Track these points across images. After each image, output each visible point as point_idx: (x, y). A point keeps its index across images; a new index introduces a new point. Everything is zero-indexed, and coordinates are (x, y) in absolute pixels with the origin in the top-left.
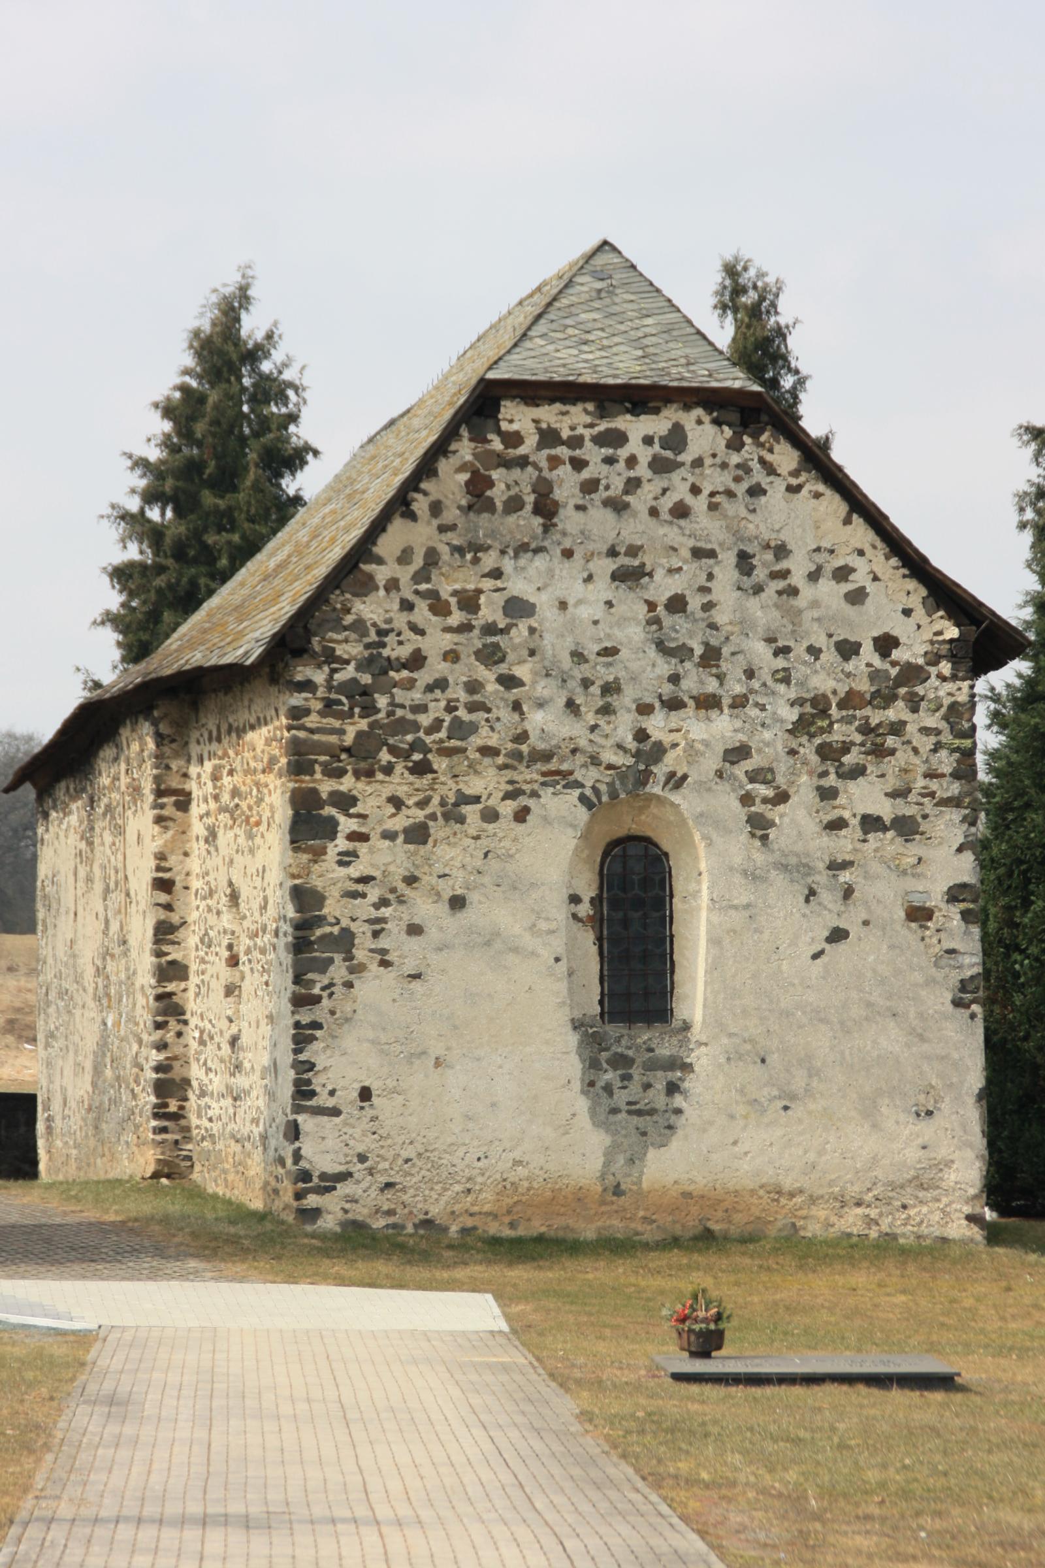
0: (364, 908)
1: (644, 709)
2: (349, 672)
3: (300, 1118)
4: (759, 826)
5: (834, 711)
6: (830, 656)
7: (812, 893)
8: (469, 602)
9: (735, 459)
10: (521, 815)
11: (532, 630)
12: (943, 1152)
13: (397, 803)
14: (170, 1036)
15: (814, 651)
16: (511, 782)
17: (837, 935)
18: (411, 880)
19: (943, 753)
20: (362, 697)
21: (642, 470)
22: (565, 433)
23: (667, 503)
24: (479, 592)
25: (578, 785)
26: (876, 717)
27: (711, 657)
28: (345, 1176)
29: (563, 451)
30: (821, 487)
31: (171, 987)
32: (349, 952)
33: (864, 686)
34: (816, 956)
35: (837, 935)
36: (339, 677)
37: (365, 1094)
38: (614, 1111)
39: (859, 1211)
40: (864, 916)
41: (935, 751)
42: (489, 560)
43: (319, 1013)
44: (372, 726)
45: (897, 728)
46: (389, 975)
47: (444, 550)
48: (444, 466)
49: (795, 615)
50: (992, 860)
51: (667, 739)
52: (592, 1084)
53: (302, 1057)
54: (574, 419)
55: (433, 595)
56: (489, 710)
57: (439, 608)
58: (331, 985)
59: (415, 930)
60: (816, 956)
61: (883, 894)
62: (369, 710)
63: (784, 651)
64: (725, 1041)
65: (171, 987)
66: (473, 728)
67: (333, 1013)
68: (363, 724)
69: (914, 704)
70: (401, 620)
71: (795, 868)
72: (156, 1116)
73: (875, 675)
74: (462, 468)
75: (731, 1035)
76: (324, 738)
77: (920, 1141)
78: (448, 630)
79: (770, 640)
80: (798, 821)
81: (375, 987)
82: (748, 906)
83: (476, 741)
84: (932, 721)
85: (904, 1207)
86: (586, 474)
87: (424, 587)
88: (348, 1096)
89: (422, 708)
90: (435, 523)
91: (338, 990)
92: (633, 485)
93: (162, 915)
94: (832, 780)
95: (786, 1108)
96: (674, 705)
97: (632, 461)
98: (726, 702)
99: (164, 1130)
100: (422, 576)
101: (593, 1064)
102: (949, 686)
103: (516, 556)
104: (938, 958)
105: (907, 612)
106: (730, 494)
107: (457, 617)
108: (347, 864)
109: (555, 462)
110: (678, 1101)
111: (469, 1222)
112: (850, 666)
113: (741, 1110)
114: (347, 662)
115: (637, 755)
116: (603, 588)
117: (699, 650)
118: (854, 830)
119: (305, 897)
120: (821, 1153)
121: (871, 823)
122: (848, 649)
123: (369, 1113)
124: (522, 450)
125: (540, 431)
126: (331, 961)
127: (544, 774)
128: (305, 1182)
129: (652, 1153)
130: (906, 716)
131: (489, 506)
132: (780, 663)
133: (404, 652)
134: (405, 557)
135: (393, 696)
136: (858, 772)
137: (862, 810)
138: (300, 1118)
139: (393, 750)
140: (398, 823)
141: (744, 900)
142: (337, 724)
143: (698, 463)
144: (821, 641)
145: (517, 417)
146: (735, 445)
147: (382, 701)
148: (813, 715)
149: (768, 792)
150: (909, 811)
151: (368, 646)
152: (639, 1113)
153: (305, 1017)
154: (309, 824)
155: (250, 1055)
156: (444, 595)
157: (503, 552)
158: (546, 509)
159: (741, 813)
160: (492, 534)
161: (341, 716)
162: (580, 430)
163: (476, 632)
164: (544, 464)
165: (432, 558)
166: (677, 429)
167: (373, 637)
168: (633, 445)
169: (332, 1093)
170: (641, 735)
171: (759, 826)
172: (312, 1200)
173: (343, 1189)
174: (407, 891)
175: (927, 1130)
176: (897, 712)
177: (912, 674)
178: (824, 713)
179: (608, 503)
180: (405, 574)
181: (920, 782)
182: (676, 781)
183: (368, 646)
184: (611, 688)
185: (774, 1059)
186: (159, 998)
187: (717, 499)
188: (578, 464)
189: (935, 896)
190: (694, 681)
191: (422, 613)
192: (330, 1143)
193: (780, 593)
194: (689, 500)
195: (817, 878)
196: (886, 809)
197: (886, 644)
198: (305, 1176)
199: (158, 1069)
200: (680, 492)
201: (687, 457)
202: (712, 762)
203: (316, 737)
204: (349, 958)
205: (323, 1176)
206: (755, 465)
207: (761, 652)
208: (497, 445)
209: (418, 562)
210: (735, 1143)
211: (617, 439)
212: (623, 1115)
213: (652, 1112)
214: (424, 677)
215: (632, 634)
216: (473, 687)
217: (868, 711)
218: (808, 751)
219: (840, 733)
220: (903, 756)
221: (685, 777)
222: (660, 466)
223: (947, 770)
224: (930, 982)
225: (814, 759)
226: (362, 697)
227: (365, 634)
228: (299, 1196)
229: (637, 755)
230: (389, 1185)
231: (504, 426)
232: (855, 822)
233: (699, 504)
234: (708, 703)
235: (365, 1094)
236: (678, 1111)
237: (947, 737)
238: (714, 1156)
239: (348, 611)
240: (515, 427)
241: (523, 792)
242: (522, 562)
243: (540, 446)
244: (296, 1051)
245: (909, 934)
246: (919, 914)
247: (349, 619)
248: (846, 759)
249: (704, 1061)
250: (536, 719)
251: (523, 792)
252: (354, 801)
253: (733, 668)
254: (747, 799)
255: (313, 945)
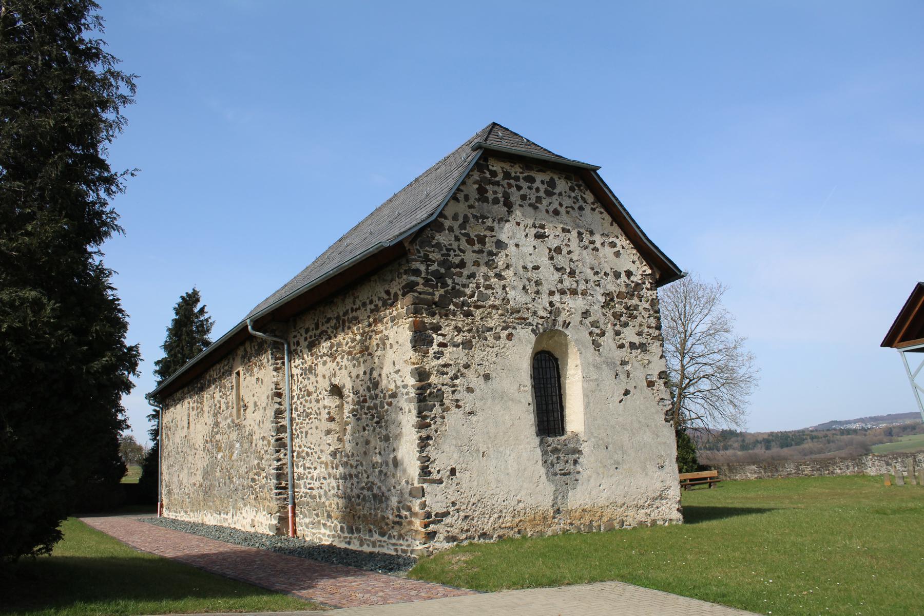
0: (446, 379)
1: (552, 293)
2: (434, 267)
3: (425, 486)
4: (597, 345)
5: (615, 299)
6: (611, 278)
8: (482, 240)
9: (573, 195)
10: (510, 337)
11: (507, 255)
12: (667, 483)
13: (458, 330)
14: (282, 456)
15: (606, 274)
16: (504, 322)
17: (627, 393)
18: (467, 366)
19: (652, 318)
20: (440, 278)
21: (542, 194)
22: (513, 175)
23: (551, 209)
24: (485, 236)
25: (530, 325)
26: (630, 303)
27: (572, 273)
28: (446, 514)
29: (512, 181)
30: (602, 210)
31: (282, 435)
32: (442, 401)
33: (623, 289)
34: (620, 402)
35: (627, 393)
36: (431, 268)
37: (453, 472)
38: (556, 474)
39: (643, 511)
42: (489, 223)
43: (431, 431)
44: (446, 292)
45: (636, 308)
46: (460, 412)
48: (470, 181)
49: (596, 257)
51: (561, 306)
52: (545, 462)
53: (424, 454)
54: (515, 170)
55: (467, 235)
56: (493, 289)
57: (470, 242)
58: (435, 417)
59: (470, 390)
60: (620, 402)
62: (444, 285)
63: (597, 273)
65: (282, 435)
66: (488, 298)
67: (436, 431)
68: (442, 291)
69: (640, 298)
70: (455, 245)
71: (610, 363)
72: (277, 488)
73: (627, 285)
74: (475, 183)
76: (426, 296)
78: (474, 252)
79: (592, 269)
80: (608, 341)
81: (454, 417)
82: (596, 380)
83: (489, 303)
84: (647, 306)
86: (522, 192)
87: (463, 231)
88: (445, 473)
89: (464, 286)
90: (467, 204)
91: (439, 420)
92: (539, 200)
93: (277, 406)
94: (617, 327)
96: (562, 292)
97: (538, 190)
98: (580, 292)
99: (280, 494)
100: (463, 226)
101: (545, 453)
102: (650, 292)
103: (499, 223)
105: (634, 262)
106: (573, 208)
107: (477, 247)
108: (438, 358)
109: (510, 186)
110: (579, 468)
111: (501, 532)
112: (618, 281)
113: (601, 470)
114: (434, 262)
115: (550, 313)
116: (532, 241)
117: (568, 270)
118: (627, 349)
119: (422, 375)
120: (629, 487)
121: (633, 346)
122: (617, 275)
123: (455, 481)
124: (497, 179)
125: (503, 172)
126: (434, 405)
127: (515, 319)
128: (428, 518)
130: (639, 303)
131: (486, 200)
132: (596, 278)
133: (457, 260)
134: (455, 217)
135: (454, 280)
136: (626, 325)
138: (425, 486)
139: (455, 305)
140: (459, 339)
141: (594, 377)
142: (431, 291)
143: (560, 194)
144: (608, 271)
145: (496, 166)
146: (572, 189)
147: (449, 281)
148: (609, 298)
149: (598, 331)
150: (644, 341)
151: (443, 255)
152: (564, 474)
153: (424, 433)
154: (421, 339)
156: (472, 236)
157: (494, 221)
158: (509, 205)
159: (590, 339)
160: (489, 212)
161: (432, 287)
162: (518, 174)
163: (485, 254)
164: (506, 186)
165: (466, 219)
166: (552, 179)
167: (444, 251)
168: (538, 184)
169: (438, 472)
170: (551, 304)
171: (597, 345)
172: (432, 528)
173: (448, 520)
174: (465, 371)
176: (635, 301)
177: (638, 286)
178: (612, 300)
179: (530, 205)
180: (456, 225)
181: (646, 330)
183: (443, 255)
185: (610, 447)
186: (277, 440)
187: (569, 209)
188: (519, 188)
190: (568, 283)
191: (463, 243)
192: (439, 498)
194: (559, 208)
196: (636, 340)
197: (629, 274)
198: (428, 515)
199: (277, 469)
200: (555, 205)
201: (557, 191)
202: (577, 318)
203: (422, 296)
204: (442, 405)
205: (436, 515)
207: (590, 273)
208: (488, 175)
209: (461, 220)
211: (531, 180)
212: (559, 476)
213: (569, 474)
214: (466, 272)
215: (544, 261)
216: (487, 278)
217: (626, 300)
218: (609, 315)
219: (619, 308)
220: (639, 319)
221: (569, 323)
222: (549, 194)
224: (657, 412)
226: (440, 278)
227: (442, 250)
228: (426, 526)
229: (550, 313)
230: (466, 517)
231: (490, 167)
232: (627, 345)
233: (562, 210)
234: (574, 292)
235: (453, 472)
236: (579, 472)
237: (652, 312)
239: (434, 238)
240: (494, 168)
241: (509, 327)
242: (501, 225)
243: (504, 179)
244: (421, 452)
245: (648, 391)
247: (434, 242)
248: (622, 319)
249: (586, 449)
250: (512, 294)
251: (509, 327)
252: (440, 328)
254: (591, 333)
255: (427, 397)
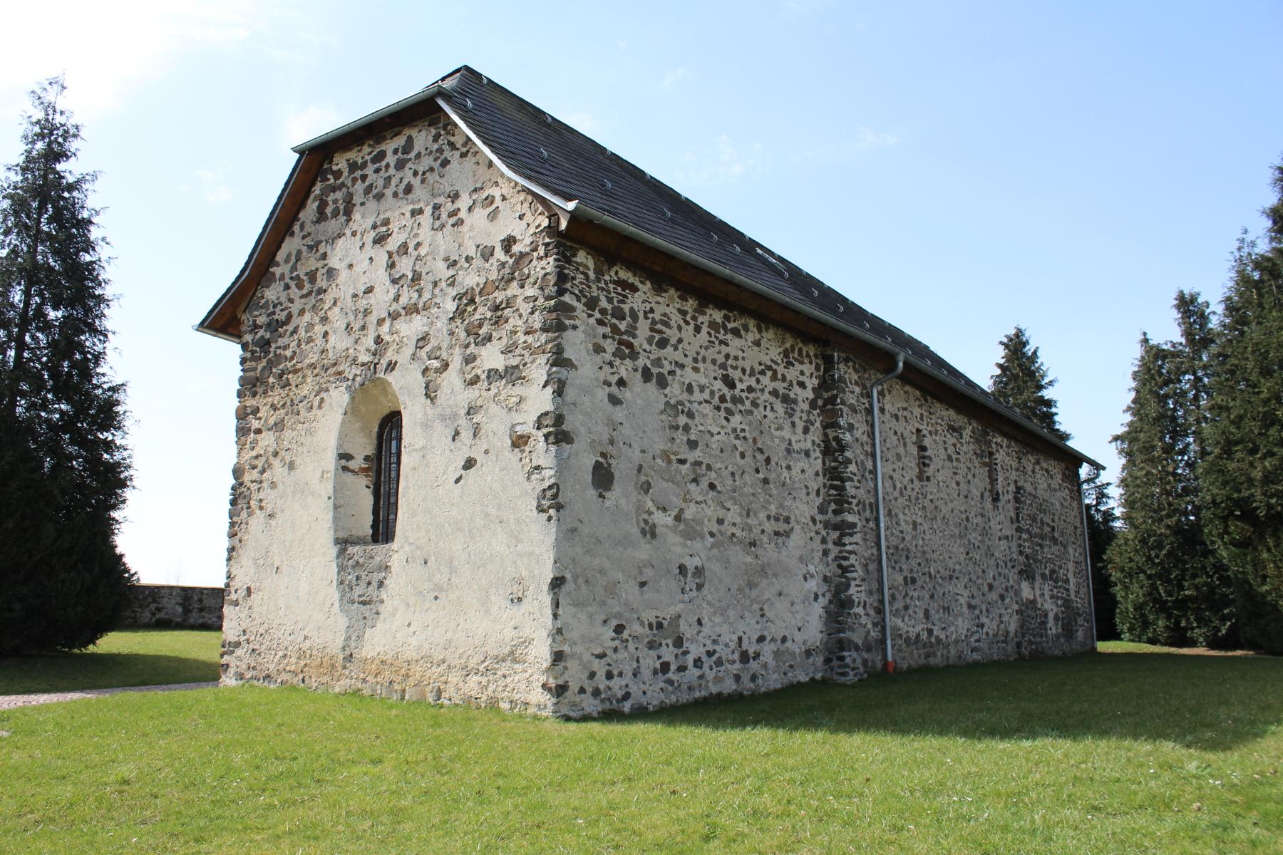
6: (478, 262)
7: (457, 433)
12: (526, 632)
15: (468, 259)
17: (469, 464)
34: (457, 481)
35: (469, 464)
40: (485, 447)
41: (532, 313)
45: (509, 303)
47: (304, 249)
50: (516, 333)
60: (457, 481)
61: (497, 424)
64: (407, 548)
75: (410, 544)
77: (513, 623)
80: (451, 381)
85: (505, 677)
95: (436, 598)
101: (341, 568)
104: (530, 474)
122: (487, 254)
129: (368, 632)
136: (489, 338)
137: (487, 367)
144: (472, 251)
155: (454, 678)
159: (421, 381)
175: (518, 613)
176: (514, 289)
182: (391, 366)
183: (269, 315)
184: (367, 312)
185: (432, 560)
189: (528, 428)
193: (453, 226)
195: (460, 422)
206: (446, 147)
210: (409, 625)
215: (380, 277)
223: (538, 325)
225: (463, 335)
238: (398, 635)
245: (512, 457)
246: (519, 442)
253: (426, 283)
